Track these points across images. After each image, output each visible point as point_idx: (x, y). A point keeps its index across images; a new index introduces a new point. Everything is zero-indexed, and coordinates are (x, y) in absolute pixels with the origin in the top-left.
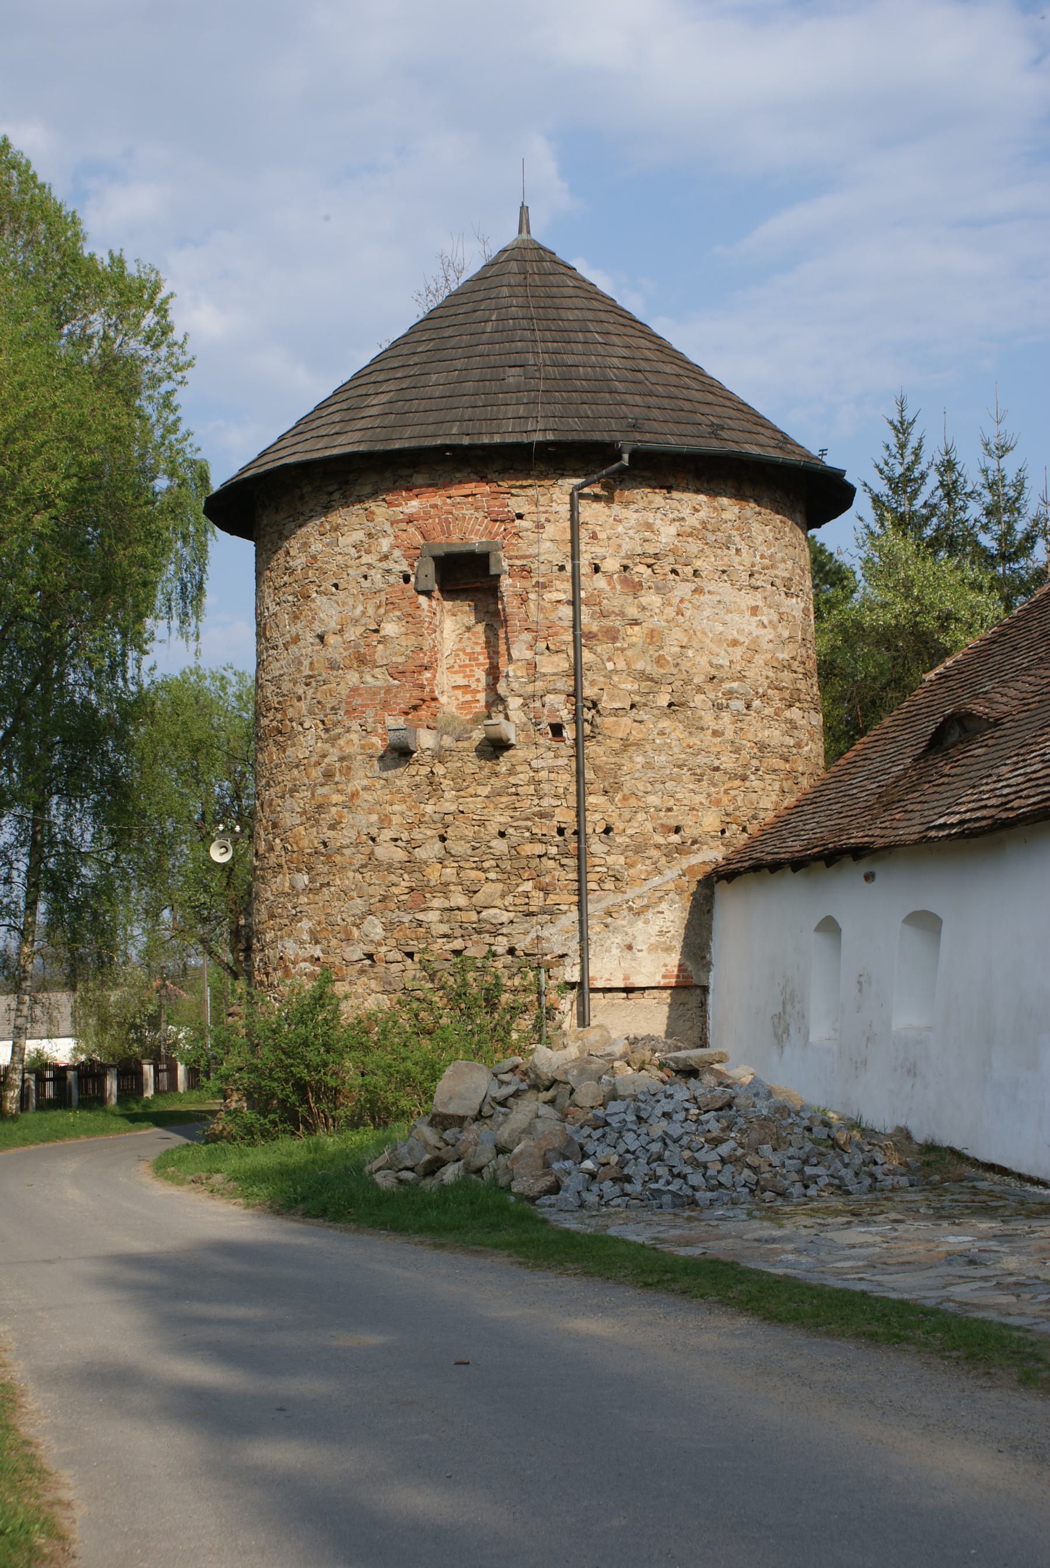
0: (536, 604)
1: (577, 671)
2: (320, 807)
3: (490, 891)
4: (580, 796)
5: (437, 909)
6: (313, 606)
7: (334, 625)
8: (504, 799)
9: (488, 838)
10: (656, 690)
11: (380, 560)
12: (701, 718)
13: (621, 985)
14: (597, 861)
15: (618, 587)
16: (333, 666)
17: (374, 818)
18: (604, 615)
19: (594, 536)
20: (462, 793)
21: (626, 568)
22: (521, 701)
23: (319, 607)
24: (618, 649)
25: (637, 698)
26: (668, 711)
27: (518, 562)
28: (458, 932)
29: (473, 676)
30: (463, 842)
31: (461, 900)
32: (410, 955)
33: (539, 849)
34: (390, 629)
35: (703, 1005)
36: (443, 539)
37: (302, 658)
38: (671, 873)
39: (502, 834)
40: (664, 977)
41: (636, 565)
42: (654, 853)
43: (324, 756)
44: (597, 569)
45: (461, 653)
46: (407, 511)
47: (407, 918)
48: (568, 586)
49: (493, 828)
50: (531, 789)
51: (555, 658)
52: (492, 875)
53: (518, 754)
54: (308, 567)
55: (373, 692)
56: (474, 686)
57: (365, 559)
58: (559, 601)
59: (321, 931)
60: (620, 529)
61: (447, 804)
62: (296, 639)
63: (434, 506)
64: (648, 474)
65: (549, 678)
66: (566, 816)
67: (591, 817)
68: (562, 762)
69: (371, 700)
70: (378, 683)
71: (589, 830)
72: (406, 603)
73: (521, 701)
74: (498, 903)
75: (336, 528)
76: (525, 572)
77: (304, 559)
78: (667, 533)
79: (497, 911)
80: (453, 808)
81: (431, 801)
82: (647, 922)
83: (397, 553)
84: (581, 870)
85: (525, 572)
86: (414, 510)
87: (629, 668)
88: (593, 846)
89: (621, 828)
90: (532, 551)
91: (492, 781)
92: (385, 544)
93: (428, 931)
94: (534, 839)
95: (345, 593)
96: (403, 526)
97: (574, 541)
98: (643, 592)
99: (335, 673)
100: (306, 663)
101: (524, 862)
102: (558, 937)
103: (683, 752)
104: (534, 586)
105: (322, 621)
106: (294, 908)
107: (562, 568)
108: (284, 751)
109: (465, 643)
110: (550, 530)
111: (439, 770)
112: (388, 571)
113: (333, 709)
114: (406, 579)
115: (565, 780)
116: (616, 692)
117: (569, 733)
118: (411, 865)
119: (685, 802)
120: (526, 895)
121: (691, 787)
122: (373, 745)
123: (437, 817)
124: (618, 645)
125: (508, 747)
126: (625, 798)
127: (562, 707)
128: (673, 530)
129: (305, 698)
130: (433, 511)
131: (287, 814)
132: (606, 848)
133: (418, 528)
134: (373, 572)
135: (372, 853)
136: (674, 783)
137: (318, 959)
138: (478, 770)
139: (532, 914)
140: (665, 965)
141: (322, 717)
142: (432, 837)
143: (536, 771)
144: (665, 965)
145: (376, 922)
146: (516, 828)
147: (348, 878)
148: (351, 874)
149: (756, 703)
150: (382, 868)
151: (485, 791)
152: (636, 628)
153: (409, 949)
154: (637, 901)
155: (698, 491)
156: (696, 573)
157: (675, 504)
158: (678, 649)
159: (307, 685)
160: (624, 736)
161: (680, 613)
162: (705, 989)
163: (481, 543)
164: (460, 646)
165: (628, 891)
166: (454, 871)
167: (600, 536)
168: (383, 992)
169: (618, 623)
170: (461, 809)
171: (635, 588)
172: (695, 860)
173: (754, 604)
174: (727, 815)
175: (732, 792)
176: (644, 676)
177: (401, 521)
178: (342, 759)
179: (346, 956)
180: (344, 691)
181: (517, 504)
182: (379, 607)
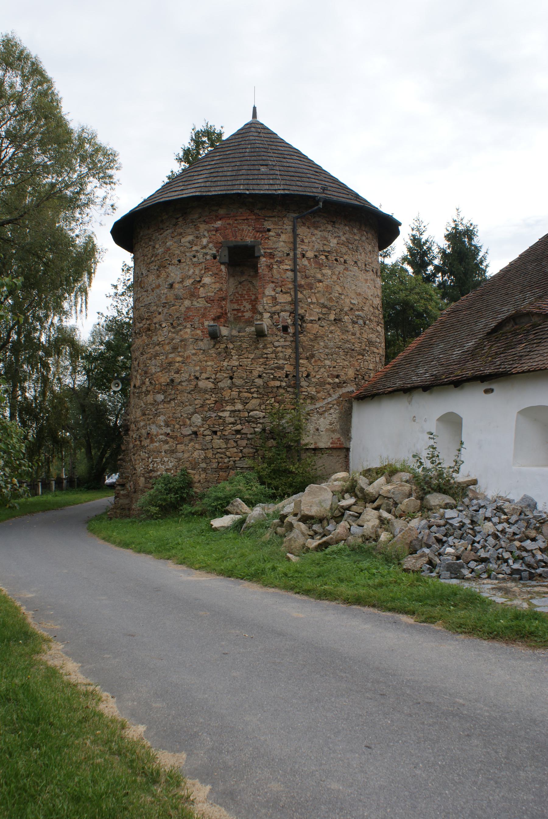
1: (295, 302)
2: (170, 364)
4: (297, 359)
5: (229, 411)
6: (167, 270)
7: (178, 279)
8: (261, 360)
9: (254, 378)
10: (328, 312)
11: (202, 249)
12: (347, 327)
14: (303, 390)
15: (313, 265)
16: (177, 298)
17: (198, 368)
18: (306, 277)
19: (302, 241)
20: (241, 357)
21: (316, 256)
22: (269, 314)
23: (171, 271)
24: (312, 293)
25: (321, 316)
26: (334, 322)
27: (269, 251)
28: (238, 422)
31: (239, 406)
32: (215, 433)
33: (278, 383)
34: (207, 280)
35: (347, 457)
36: (233, 239)
37: (161, 295)
38: (335, 396)
39: (260, 376)
40: (331, 443)
41: (320, 255)
42: (328, 386)
43: (173, 339)
44: (303, 256)
46: (215, 226)
47: (214, 415)
49: (256, 373)
51: (285, 296)
52: (255, 395)
54: (165, 253)
55: (197, 309)
56: (242, 309)
58: (287, 270)
59: (170, 421)
60: (314, 239)
62: (159, 286)
63: (229, 224)
65: (282, 305)
66: (288, 368)
68: (287, 343)
69: (197, 313)
70: (201, 305)
71: (300, 376)
73: (269, 314)
74: (258, 408)
75: (181, 234)
76: (271, 256)
77: (163, 250)
79: (258, 412)
80: (237, 363)
81: (226, 360)
83: (211, 245)
85: (271, 256)
86: (219, 226)
87: (317, 302)
88: (302, 383)
89: (314, 375)
91: (255, 352)
92: (205, 241)
93: (224, 421)
94: (275, 379)
95: (185, 264)
98: (323, 268)
99: (179, 301)
103: (340, 342)
104: (276, 262)
106: (156, 410)
107: (288, 255)
108: (151, 338)
110: (283, 237)
113: (177, 318)
114: (215, 257)
116: (312, 312)
117: (291, 330)
119: (341, 364)
120: (271, 405)
121: (343, 357)
122: (198, 334)
123: (229, 368)
124: (313, 291)
125: (265, 336)
126: (315, 361)
127: (288, 318)
128: (335, 241)
129: (163, 313)
130: (228, 227)
131: (153, 367)
132: (307, 384)
134: (198, 254)
135: (197, 384)
136: (336, 356)
137: (169, 434)
140: (332, 438)
141: (171, 321)
142: (226, 377)
143: (276, 347)
144: (332, 438)
145: (199, 416)
146: (266, 373)
147: (184, 396)
148: (186, 394)
149: (367, 322)
150: (201, 392)
151: (252, 356)
152: (321, 284)
153: (214, 429)
154: (321, 409)
155: (345, 225)
156: (345, 262)
157: (336, 230)
158: (338, 295)
159: (163, 307)
160: (315, 333)
161: (338, 278)
162: (348, 450)
163: (251, 241)
165: (317, 404)
166: (237, 393)
167: (306, 241)
168: (202, 449)
169: (313, 281)
170: (241, 364)
171: (320, 266)
173: (366, 278)
174: (357, 371)
175: (359, 361)
176: (324, 306)
177: (213, 230)
178: (182, 341)
179: (183, 433)
180: (183, 309)
181: (268, 225)
182: (202, 270)
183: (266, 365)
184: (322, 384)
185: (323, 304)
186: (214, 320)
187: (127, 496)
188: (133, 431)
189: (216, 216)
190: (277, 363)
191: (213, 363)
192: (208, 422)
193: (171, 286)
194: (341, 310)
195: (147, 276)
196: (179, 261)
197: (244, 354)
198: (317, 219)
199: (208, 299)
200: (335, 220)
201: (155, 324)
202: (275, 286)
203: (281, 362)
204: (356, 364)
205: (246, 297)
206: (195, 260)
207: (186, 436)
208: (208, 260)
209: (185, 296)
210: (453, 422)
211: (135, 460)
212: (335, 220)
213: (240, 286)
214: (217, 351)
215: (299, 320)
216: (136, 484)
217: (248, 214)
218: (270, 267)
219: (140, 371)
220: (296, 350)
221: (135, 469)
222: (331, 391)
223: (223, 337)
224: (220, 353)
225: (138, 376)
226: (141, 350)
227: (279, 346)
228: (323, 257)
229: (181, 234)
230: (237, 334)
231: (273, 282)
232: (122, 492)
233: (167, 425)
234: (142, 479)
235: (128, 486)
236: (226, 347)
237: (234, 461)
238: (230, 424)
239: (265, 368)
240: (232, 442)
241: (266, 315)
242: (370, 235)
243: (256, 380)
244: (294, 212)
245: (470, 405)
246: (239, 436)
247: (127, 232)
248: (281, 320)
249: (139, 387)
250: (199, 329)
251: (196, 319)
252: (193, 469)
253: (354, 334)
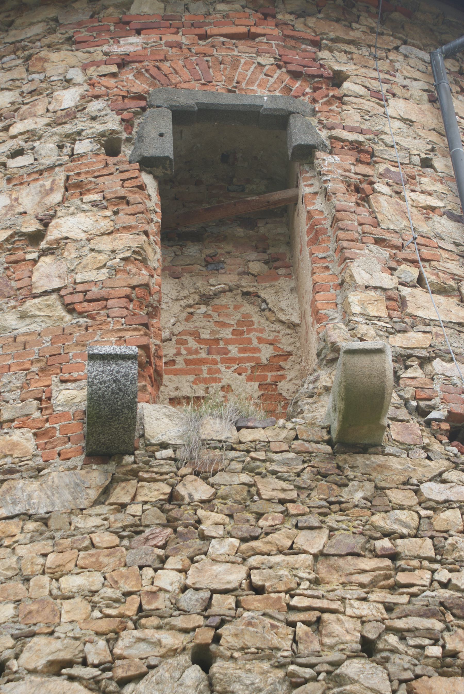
8: (368, 563)
9: (335, 656)
29: (215, 380)
30: (266, 665)
34: (72, 224)
39: (368, 648)
45: (190, 339)
49: (344, 631)
50: (427, 548)
61: (218, 568)
80: (235, 576)
81: (174, 562)
83: (95, 106)
85: (362, 152)
91: (331, 520)
109: (199, 322)
114: (111, 146)
122: (15, 445)
123: (189, 600)
130: (172, 52)
138: (293, 495)
142: (174, 652)
146: (402, 634)
151: (316, 542)
164: (189, 326)
170: (256, 579)
183: (395, 587)
190: (445, 585)
191: (97, 578)
197: (274, 529)
199: (79, 297)
202: (393, 257)
205: (234, 350)
208: (82, 156)
213: (203, 309)
214: (120, 520)
217: (251, 21)
224: (136, 529)
227: (447, 504)
230: (228, 433)
236: (173, 497)
239: (389, 608)
243: (352, 668)
248: (437, 387)
250: (23, 422)
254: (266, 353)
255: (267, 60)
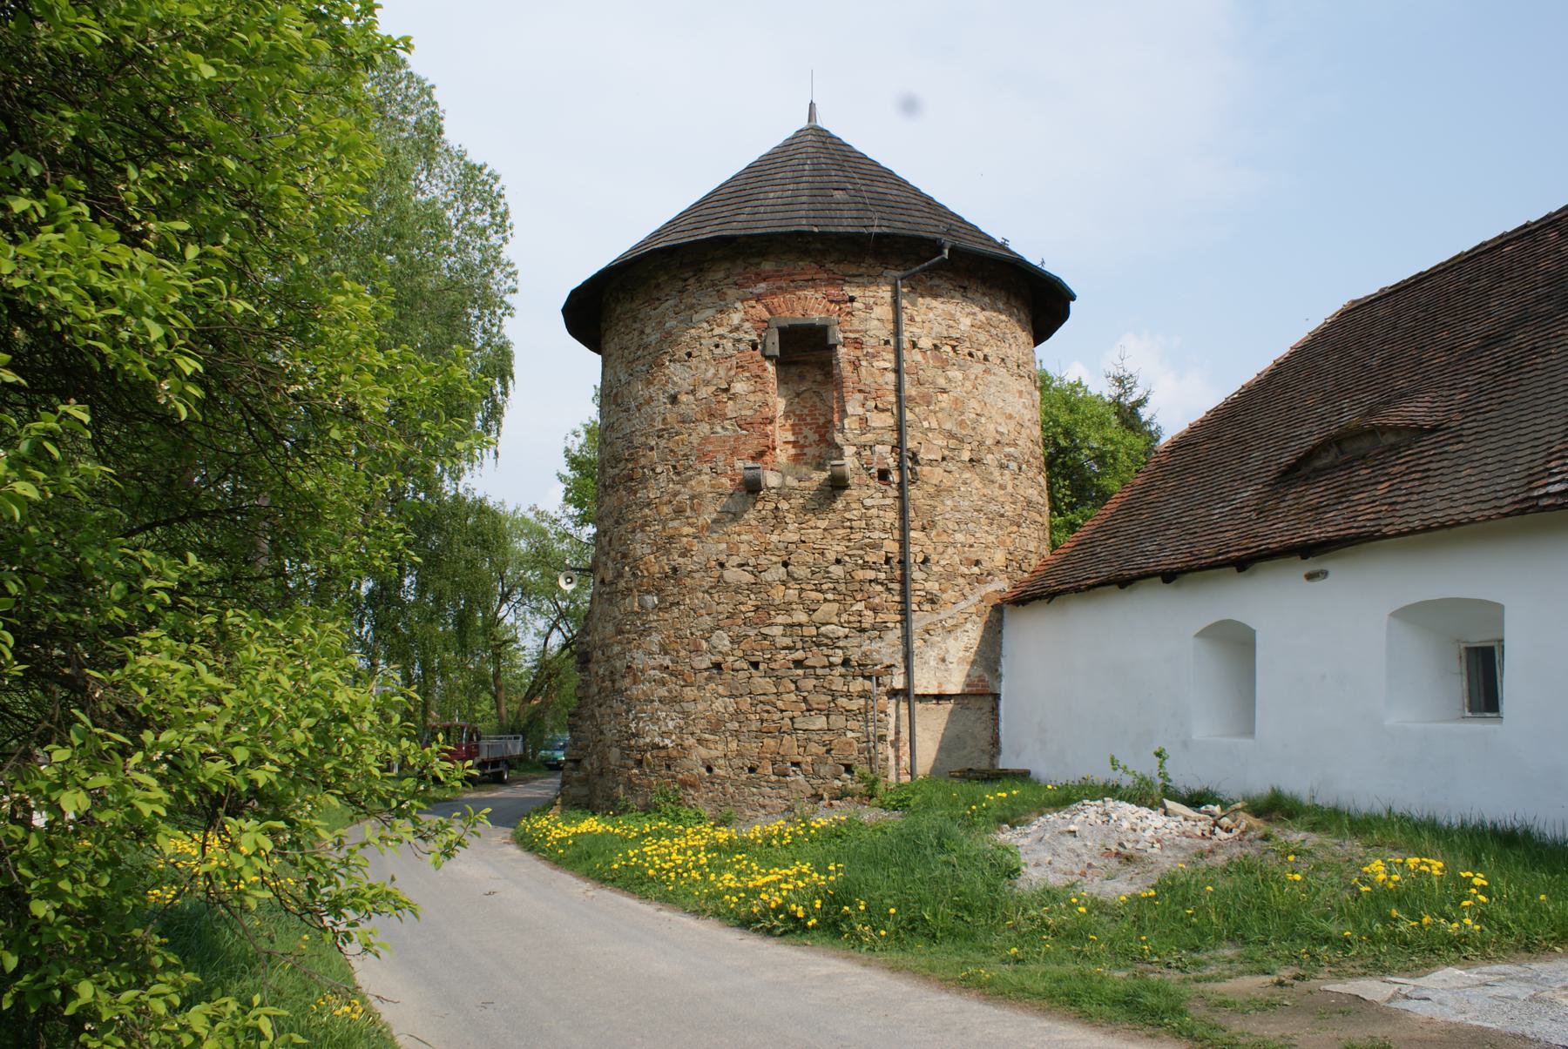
0: (866, 373)
1: (900, 428)
3: (828, 610)
8: (841, 531)
13: (933, 691)
14: (918, 586)
19: (912, 319)
21: (935, 346)
27: (852, 335)
28: (799, 645)
31: (802, 617)
32: (755, 665)
33: (871, 575)
34: (739, 387)
35: (995, 710)
38: (974, 599)
39: (838, 561)
42: (961, 581)
43: (675, 495)
44: (914, 345)
47: (752, 633)
48: (891, 357)
49: (831, 556)
51: (883, 415)
52: (830, 596)
53: (853, 493)
57: (717, 331)
64: (950, 275)
66: (892, 547)
67: (914, 549)
68: (889, 501)
72: (755, 366)
74: (835, 620)
75: (692, 307)
76: (858, 344)
78: (965, 323)
80: (796, 538)
82: (956, 639)
83: (747, 325)
84: (904, 593)
85: (858, 344)
90: (862, 327)
93: (773, 643)
96: (753, 303)
97: (897, 322)
100: (659, 419)
101: (857, 586)
102: (886, 650)
105: (675, 384)
107: (887, 342)
111: (784, 505)
112: (739, 340)
114: (754, 347)
115: (891, 517)
117: (894, 477)
118: (756, 587)
123: (781, 545)
125: (847, 487)
132: (924, 576)
133: (766, 306)
135: (721, 576)
139: (863, 630)
148: (700, 595)
153: (754, 659)
155: (984, 294)
156: (986, 358)
162: (997, 697)
172: (990, 588)
176: (951, 435)
178: (692, 498)
180: (695, 440)
184: (949, 576)
185: (949, 432)
186: (753, 458)
187: (585, 781)
188: (598, 662)
189: (757, 275)
192: (743, 646)
193: (674, 399)
194: (981, 444)
195: (629, 383)
196: (689, 355)
198: (936, 281)
200: (966, 283)
201: (643, 467)
203: (876, 535)
204: (1008, 541)
206: (717, 351)
207: (700, 671)
209: (699, 416)
210: (1237, 643)
211: (602, 716)
212: (966, 283)
215: (907, 459)
216: (603, 758)
218: (856, 366)
219: (612, 554)
220: (903, 513)
221: (602, 733)
222: (967, 590)
223: (769, 489)
224: (764, 519)
225: (610, 564)
226: (616, 515)
228: (949, 349)
229: (692, 307)
231: (860, 391)
232: (575, 774)
233: (664, 651)
234: (615, 751)
235: (586, 763)
237: (792, 719)
238: (784, 648)
240: (786, 682)
241: (849, 450)
242: (1022, 316)
243: (832, 568)
244: (896, 268)
245: (1276, 606)
246: (800, 672)
247: (592, 311)
249: (612, 583)
251: (721, 457)
252: (713, 732)
253: (1002, 487)
254: (822, 421)
255: (819, 295)
